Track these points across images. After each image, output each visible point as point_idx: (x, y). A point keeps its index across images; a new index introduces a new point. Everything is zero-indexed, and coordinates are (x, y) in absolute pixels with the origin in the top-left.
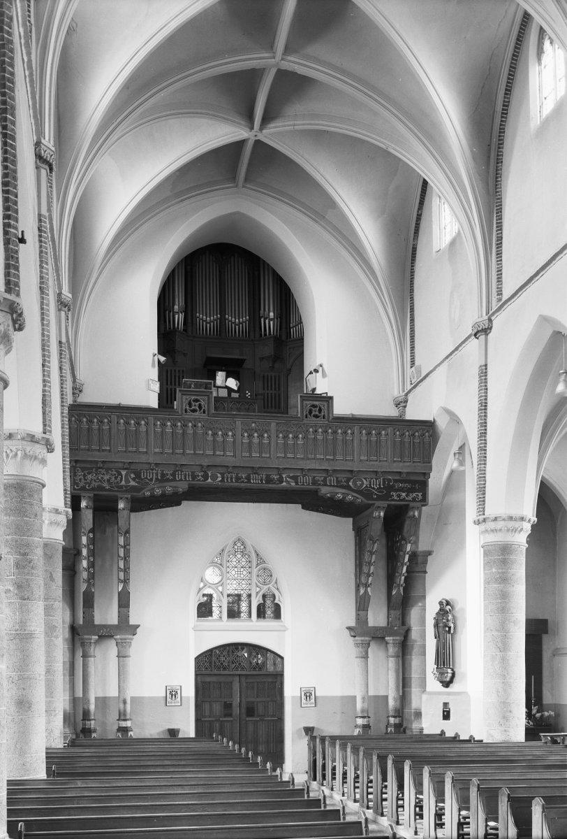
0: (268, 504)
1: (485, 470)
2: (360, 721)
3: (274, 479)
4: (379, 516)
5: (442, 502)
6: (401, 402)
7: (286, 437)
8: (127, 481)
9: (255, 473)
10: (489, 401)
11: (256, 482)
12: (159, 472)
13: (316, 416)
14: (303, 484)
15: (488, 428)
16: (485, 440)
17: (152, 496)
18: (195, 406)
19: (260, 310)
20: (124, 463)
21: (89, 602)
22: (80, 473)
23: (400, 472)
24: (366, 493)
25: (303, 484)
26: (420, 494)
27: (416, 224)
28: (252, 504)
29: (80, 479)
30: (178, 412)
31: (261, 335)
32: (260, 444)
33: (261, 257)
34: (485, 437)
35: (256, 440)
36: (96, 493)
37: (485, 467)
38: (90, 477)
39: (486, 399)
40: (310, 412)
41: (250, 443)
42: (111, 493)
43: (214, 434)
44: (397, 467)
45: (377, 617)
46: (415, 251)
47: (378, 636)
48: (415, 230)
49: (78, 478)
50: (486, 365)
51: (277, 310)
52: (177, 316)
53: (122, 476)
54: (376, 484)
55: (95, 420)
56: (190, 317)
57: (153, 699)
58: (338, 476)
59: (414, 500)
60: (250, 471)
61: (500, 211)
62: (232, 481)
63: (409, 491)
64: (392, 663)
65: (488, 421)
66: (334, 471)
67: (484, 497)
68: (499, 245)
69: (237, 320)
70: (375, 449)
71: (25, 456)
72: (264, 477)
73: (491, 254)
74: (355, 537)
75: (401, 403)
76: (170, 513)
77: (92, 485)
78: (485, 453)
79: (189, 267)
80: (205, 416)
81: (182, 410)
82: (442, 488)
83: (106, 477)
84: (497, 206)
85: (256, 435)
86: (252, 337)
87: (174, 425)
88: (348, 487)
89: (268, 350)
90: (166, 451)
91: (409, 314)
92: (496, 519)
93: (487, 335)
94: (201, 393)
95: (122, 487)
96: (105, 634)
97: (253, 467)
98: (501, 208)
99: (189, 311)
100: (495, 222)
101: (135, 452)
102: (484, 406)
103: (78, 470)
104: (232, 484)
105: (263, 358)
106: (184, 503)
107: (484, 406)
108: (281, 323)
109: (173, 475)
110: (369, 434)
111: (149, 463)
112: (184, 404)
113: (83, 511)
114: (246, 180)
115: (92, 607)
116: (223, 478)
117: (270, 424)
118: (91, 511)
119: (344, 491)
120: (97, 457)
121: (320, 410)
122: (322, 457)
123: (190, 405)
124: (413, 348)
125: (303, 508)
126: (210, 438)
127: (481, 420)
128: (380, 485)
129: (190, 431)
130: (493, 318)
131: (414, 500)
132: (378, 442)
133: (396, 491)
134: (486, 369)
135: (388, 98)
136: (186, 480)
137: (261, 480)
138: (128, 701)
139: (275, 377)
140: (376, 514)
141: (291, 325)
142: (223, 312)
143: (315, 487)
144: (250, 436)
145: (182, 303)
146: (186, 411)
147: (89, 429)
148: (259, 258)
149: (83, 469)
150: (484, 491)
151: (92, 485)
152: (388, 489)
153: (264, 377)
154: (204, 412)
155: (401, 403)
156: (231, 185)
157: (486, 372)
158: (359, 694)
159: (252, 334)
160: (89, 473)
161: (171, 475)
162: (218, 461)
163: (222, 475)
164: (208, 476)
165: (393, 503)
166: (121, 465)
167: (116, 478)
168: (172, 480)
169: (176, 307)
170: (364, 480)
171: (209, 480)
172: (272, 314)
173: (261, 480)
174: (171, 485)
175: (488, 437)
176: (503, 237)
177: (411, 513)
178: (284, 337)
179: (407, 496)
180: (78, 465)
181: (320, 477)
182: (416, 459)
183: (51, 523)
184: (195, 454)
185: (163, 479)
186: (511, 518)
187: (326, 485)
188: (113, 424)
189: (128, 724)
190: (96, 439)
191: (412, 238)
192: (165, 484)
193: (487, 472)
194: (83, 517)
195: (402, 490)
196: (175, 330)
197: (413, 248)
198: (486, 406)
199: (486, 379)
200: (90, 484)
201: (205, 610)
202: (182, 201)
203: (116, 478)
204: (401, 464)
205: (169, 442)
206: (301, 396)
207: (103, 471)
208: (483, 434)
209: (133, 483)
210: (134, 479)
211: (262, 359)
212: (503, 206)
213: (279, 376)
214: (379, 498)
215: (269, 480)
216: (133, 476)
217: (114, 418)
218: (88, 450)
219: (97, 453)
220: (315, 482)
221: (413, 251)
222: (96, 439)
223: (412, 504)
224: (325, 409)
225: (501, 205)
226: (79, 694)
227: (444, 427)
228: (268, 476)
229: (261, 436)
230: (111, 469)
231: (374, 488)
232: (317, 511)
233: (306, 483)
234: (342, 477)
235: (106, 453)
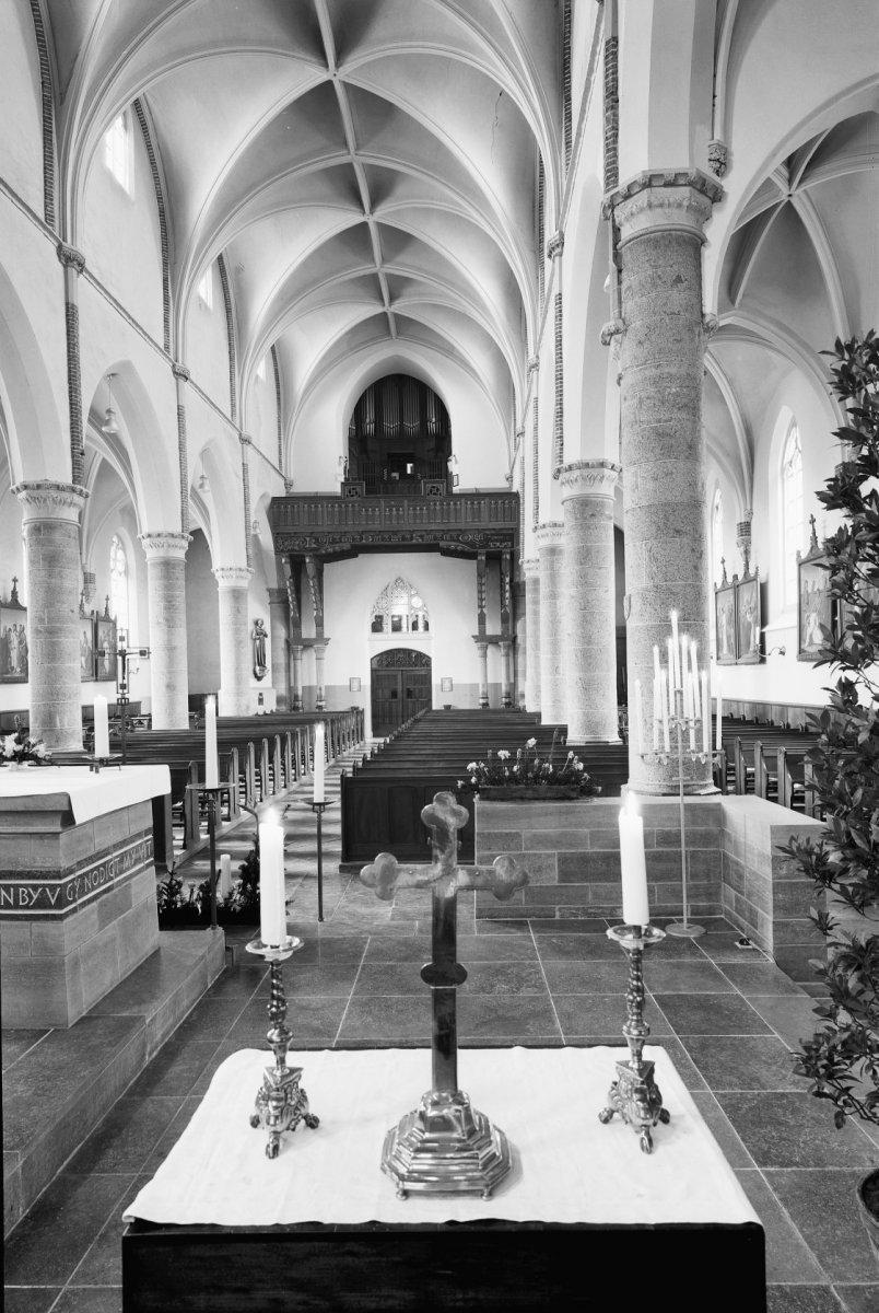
2: (481, 701)
7: (415, 509)
11: (395, 540)
18: (353, 492)
21: (298, 625)
24: (472, 544)
35: (394, 513)
44: (491, 526)
45: (494, 628)
47: (494, 641)
54: (478, 537)
57: (340, 687)
63: (501, 542)
64: (503, 660)
70: (477, 514)
71: (169, 546)
76: (351, 562)
87: (340, 506)
89: (432, 444)
96: (308, 645)
99: (378, 421)
106: (361, 556)
114: (398, 333)
115: (300, 627)
120: (291, 529)
135: (453, 284)
138: (323, 689)
142: (402, 420)
145: (372, 417)
152: (487, 540)
158: (479, 680)
162: (370, 527)
169: (368, 420)
181: (439, 535)
185: (334, 542)
189: (323, 703)
195: (497, 541)
201: (377, 626)
214: (481, 547)
215: (404, 539)
226: (512, 681)
229: (398, 510)
233: (429, 539)
234: (454, 534)
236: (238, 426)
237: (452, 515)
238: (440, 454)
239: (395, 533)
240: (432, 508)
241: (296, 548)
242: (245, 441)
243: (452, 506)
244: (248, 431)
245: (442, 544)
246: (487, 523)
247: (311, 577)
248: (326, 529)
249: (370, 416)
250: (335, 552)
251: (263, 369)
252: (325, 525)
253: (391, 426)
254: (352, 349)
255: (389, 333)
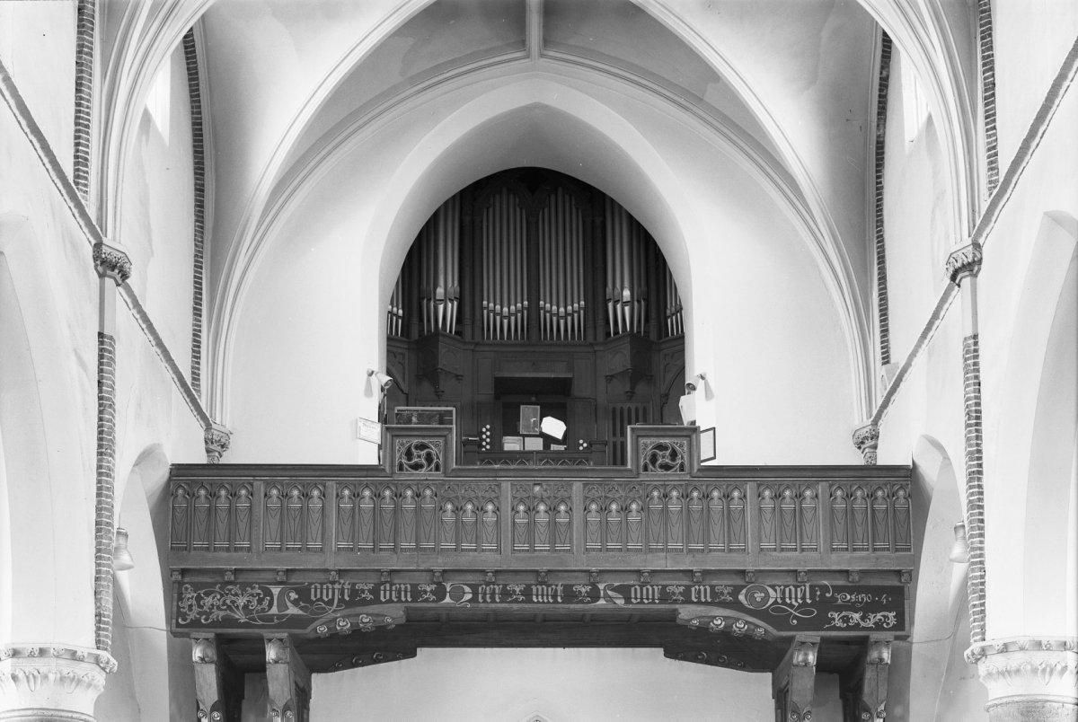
0: (629, 650)
1: (981, 549)
3: (580, 592)
4: (806, 664)
5: (954, 634)
6: (866, 438)
7: (604, 510)
8: (282, 606)
9: (541, 583)
10: (983, 408)
11: (542, 601)
12: (346, 586)
13: (666, 467)
14: (642, 602)
15: (985, 461)
16: (980, 486)
17: (334, 636)
19: (605, 285)
20: (276, 571)
22: (190, 594)
23: (847, 571)
24: (775, 616)
25: (642, 602)
26: (891, 615)
27: (880, 96)
28: (561, 649)
29: (191, 606)
30: (384, 470)
31: (608, 334)
32: (552, 525)
33: (607, 193)
34: (979, 479)
35: (542, 518)
36: (220, 631)
37: (981, 542)
38: (208, 601)
39: (978, 404)
40: (654, 459)
41: (531, 525)
42: (250, 631)
43: (458, 510)
44: (837, 561)
46: (883, 148)
48: (879, 108)
49: (185, 604)
50: (975, 337)
51: (639, 286)
52: (441, 308)
53: (272, 599)
54: (797, 596)
55: (223, 493)
56: (467, 309)
58: (714, 582)
59: (879, 627)
60: (531, 580)
61: (988, 34)
62: (485, 601)
63: (867, 609)
65: (984, 448)
66: (706, 573)
67: (983, 605)
68: (990, 99)
69: (562, 310)
72: (560, 589)
73: (975, 117)
74: (776, 709)
75: (867, 441)
77: (213, 617)
78: (981, 514)
79: (467, 219)
80: (439, 476)
81: (392, 465)
82: (950, 602)
83: (241, 601)
84: (981, 26)
85: (542, 507)
86: (590, 339)
87: (377, 496)
88: (736, 605)
89: (620, 360)
90: (362, 545)
91: (876, 267)
92: (1005, 649)
93: (975, 276)
94: (433, 434)
95: (270, 618)
97: (537, 571)
98: (990, 29)
99: (468, 298)
100: (979, 56)
101: (300, 549)
102: (975, 418)
103: (187, 589)
104: (493, 605)
105: (612, 376)
106: (423, 652)
107: (975, 418)
108: (647, 306)
109: (375, 592)
110: (778, 496)
111: (327, 571)
112: (398, 455)
113: (198, 668)
114: (547, 42)
116: (475, 593)
117: (571, 485)
118: (212, 667)
119: (728, 612)
121: (674, 455)
122: (679, 546)
123: (409, 455)
124: (885, 332)
125: (667, 655)
126: (449, 517)
127: (970, 446)
128: (803, 598)
129: (409, 505)
130: (981, 241)
131: (879, 627)
132: (799, 513)
133: (839, 609)
134: (976, 344)
136: (400, 601)
137: (554, 597)
139: (637, 410)
140: (798, 658)
141: (668, 312)
142: (534, 296)
143: (667, 606)
144: (531, 510)
145: (453, 285)
146: (401, 468)
147: (209, 509)
148: (604, 194)
149: (196, 587)
150: (982, 590)
151: (213, 617)
152: (822, 605)
153: (614, 411)
154: (437, 468)
155: (867, 441)
156: (518, 54)
157: (976, 351)
159: (590, 332)
160: (207, 594)
161: (370, 591)
162: (463, 561)
163: (474, 588)
164: (446, 592)
165: (834, 633)
166: (269, 576)
167: (260, 601)
168: (371, 603)
169: (440, 291)
170: (770, 590)
171: (448, 600)
172: (627, 293)
173: (554, 597)
174: (370, 612)
175: (987, 480)
176: (996, 82)
177: (874, 655)
178: (653, 336)
179: (863, 618)
180: (187, 580)
181: (676, 586)
182: (879, 545)
183: (62, 679)
184: (418, 549)
186: (1038, 645)
187: (688, 601)
188: (256, 496)
190: (222, 527)
191: (875, 124)
192: (358, 609)
193: (986, 552)
194: (200, 680)
195: (852, 607)
196: (436, 335)
197: (878, 142)
198: (978, 418)
199: (975, 364)
200: (208, 614)
202: (419, 92)
203: (260, 601)
204: (847, 555)
205: (366, 529)
206: (633, 429)
207: (236, 589)
208: (976, 475)
209: (293, 610)
210: (295, 603)
211: (610, 378)
212: (994, 25)
213: (645, 409)
214: (804, 625)
215: (570, 595)
216: (293, 596)
217: (260, 487)
218: (208, 549)
219: (225, 554)
220: (665, 597)
221: (878, 148)
222: (222, 527)
223: (874, 636)
224: (683, 452)
225: (990, 22)
227: (935, 478)
228: (568, 588)
229: (553, 510)
230: (251, 585)
231: (791, 606)
232: (695, 660)
233: (646, 600)
234: (724, 585)
235: (240, 553)
236: (92, 212)
237: (717, 529)
238: (641, 388)
239: (542, 577)
240: (656, 506)
241: (240, 616)
242: (111, 267)
243: (717, 505)
244: (120, 240)
245: (686, 613)
246: (823, 552)
247: (280, 704)
248: (332, 562)
249: (446, 284)
250: (356, 633)
251: (158, 94)
252: (330, 547)
253: (503, 309)
254: (413, 81)
255: (522, 43)
